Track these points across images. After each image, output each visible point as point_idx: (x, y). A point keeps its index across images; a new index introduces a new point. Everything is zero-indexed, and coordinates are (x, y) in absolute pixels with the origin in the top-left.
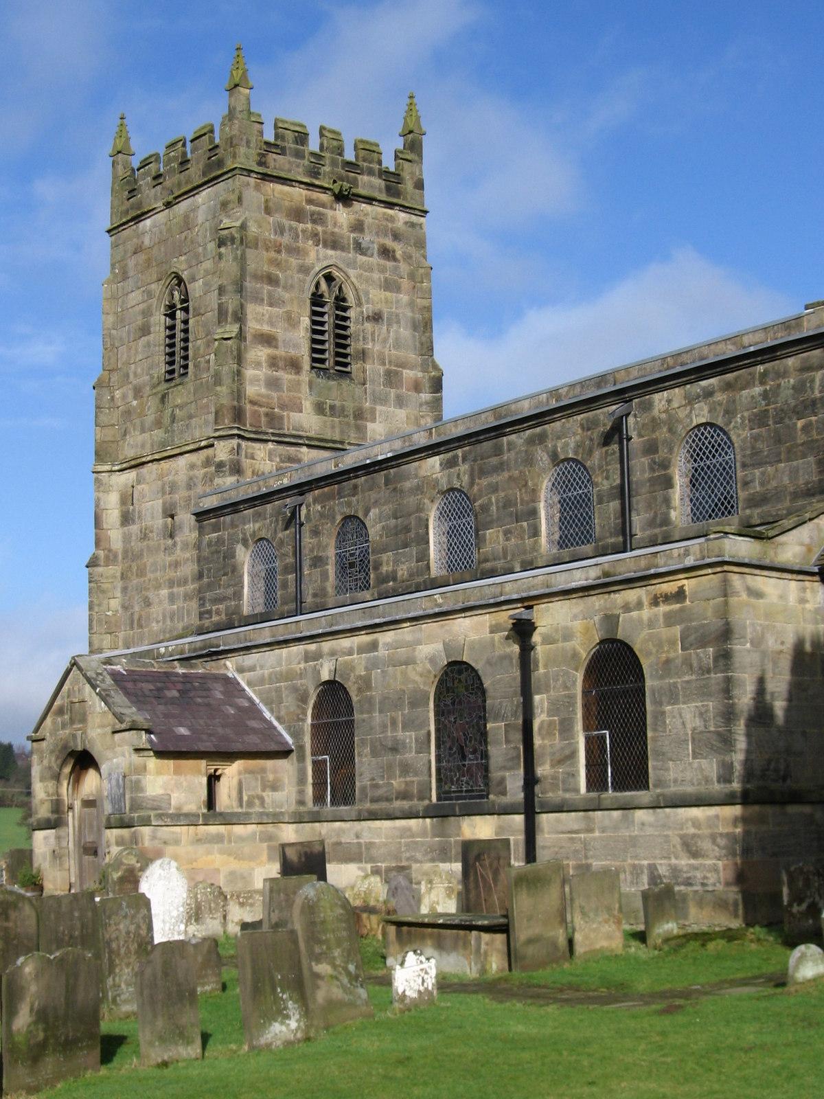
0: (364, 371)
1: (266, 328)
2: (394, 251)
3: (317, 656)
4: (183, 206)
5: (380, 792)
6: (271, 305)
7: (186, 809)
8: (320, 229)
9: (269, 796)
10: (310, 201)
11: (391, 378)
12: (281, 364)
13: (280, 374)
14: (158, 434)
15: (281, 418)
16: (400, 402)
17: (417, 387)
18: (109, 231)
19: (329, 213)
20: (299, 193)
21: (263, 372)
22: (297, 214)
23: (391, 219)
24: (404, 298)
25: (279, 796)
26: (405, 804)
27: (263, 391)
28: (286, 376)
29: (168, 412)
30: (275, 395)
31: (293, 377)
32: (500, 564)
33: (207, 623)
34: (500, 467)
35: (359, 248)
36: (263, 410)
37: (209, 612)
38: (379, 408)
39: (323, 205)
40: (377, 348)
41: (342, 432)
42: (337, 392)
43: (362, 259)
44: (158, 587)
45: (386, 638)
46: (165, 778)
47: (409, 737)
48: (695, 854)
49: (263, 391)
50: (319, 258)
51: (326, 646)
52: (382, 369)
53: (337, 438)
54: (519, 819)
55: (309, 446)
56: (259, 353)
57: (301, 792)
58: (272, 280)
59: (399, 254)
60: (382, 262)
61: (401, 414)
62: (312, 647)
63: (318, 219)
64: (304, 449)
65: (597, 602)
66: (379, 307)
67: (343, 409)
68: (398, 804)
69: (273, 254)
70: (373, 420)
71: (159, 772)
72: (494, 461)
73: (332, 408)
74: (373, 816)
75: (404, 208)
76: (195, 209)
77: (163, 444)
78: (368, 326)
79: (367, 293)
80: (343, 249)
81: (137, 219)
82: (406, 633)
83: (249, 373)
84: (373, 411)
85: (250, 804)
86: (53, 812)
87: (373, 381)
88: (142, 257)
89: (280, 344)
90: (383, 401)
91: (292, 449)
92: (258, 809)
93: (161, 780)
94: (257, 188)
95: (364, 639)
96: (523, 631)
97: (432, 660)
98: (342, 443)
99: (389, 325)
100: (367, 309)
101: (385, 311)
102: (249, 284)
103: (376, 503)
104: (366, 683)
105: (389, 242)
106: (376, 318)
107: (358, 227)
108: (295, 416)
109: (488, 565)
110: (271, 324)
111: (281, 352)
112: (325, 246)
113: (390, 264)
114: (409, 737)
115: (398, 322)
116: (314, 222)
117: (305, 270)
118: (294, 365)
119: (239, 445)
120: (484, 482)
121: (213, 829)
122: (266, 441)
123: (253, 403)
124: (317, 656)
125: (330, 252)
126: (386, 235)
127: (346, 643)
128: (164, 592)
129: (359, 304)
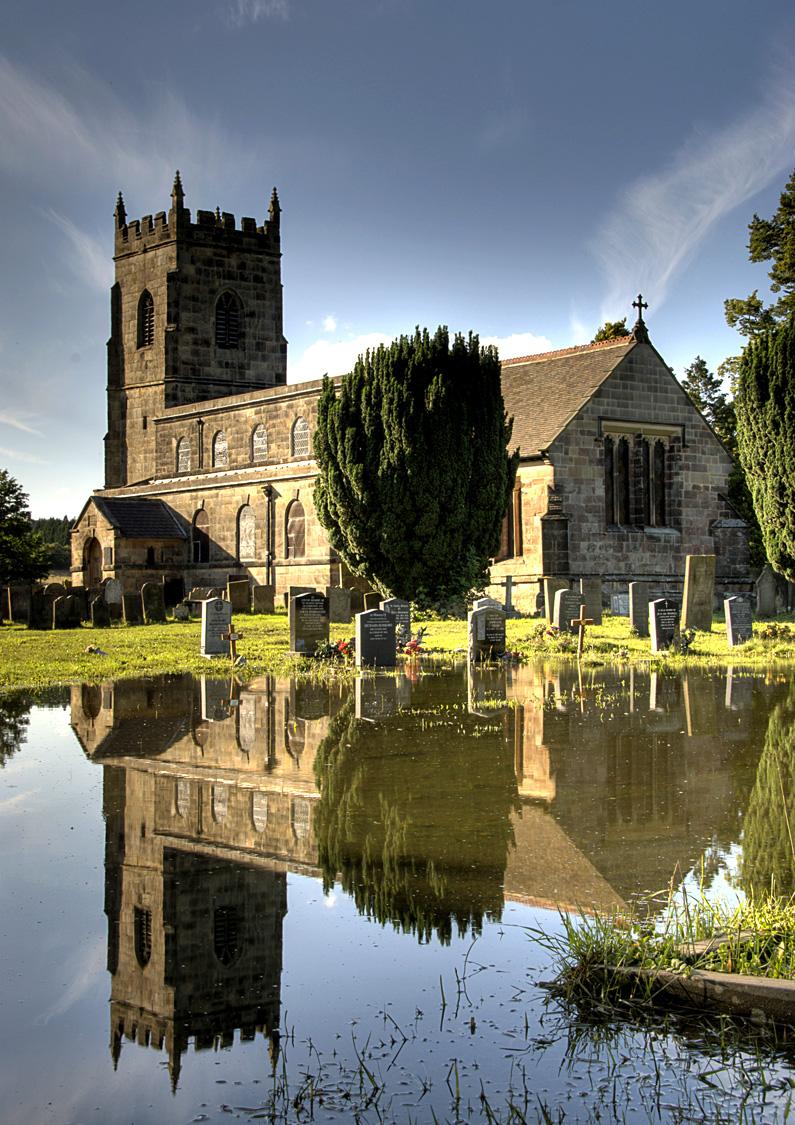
0: (244, 343)
1: (192, 324)
2: (262, 278)
3: (196, 498)
4: (151, 254)
5: (218, 557)
6: (194, 312)
7: (137, 563)
8: (221, 269)
9: (175, 558)
10: (215, 254)
11: (260, 346)
12: (200, 342)
13: (199, 347)
14: (139, 373)
15: (199, 370)
16: (264, 358)
17: (274, 350)
18: (114, 259)
19: (226, 260)
20: (209, 252)
21: (188, 348)
22: (209, 262)
23: (261, 260)
24: (267, 303)
25: (179, 558)
26: (227, 562)
27: (191, 358)
28: (202, 349)
29: (144, 363)
30: (196, 359)
31: (206, 349)
32: (275, 459)
33: (159, 474)
34: (277, 417)
35: (243, 278)
36: (189, 367)
37: (160, 470)
38: (252, 362)
39: (224, 256)
40: (252, 331)
41: (232, 376)
42: (229, 355)
43: (243, 283)
44: (140, 453)
45: (222, 492)
46: (128, 550)
47: (228, 534)
48: (318, 583)
49: (191, 358)
50: (222, 286)
51: (200, 493)
52: (254, 342)
53: (229, 379)
54: (264, 569)
55: (214, 384)
56: (189, 337)
57: (189, 557)
58: (194, 299)
59: (265, 279)
60: (255, 284)
61: (265, 365)
62: (194, 494)
63: (220, 264)
64: (211, 386)
65: (292, 484)
66: (252, 309)
67: (232, 364)
68: (224, 562)
69: (195, 285)
70: (249, 369)
71: (126, 547)
72: (274, 413)
73: (227, 364)
74: (216, 567)
75: (268, 254)
76: (156, 256)
77: (142, 380)
78: (247, 319)
79: (246, 302)
80: (234, 279)
81: (129, 255)
82: (228, 491)
83: (181, 348)
84: (249, 364)
85: (167, 561)
86: (712, 877)
87: (249, 349)
88: (129, 278)
89: (199, 332)
90: (256, 359)
91: (204, 387)
92: (170, 563)
93: (126, 551)
94: (187, 250)
95: (214, 492)
96: (271, 493)
97: (237, 502)
98: (232, 381)
99: (259, 318)
100: (247, 310)
101: (257, 310)
102: (181, 303)
103: (230, 425)
104: (213, 511)
105: (260, 273)
106: (252, 315)
107: (242, 266)
108: (206, 369)
109: (271, 459)
110: (194, 322)
111: (200, 336)
112: (224, 278)
113: (259, 285)
114: (228, 534)
115: (264, 316)
116: (218, 265)
117: (213, 292)
118: (207, 343)
119: (177, 386)
120: (271, 422)
121: (150, 572)
122: (191, 383)
123: (184, 363)
124: (196, 498)
125: (227, 281)
126: (258, 270)
127: (206, 493)
128: (142, 456)
129: (242, 308)
